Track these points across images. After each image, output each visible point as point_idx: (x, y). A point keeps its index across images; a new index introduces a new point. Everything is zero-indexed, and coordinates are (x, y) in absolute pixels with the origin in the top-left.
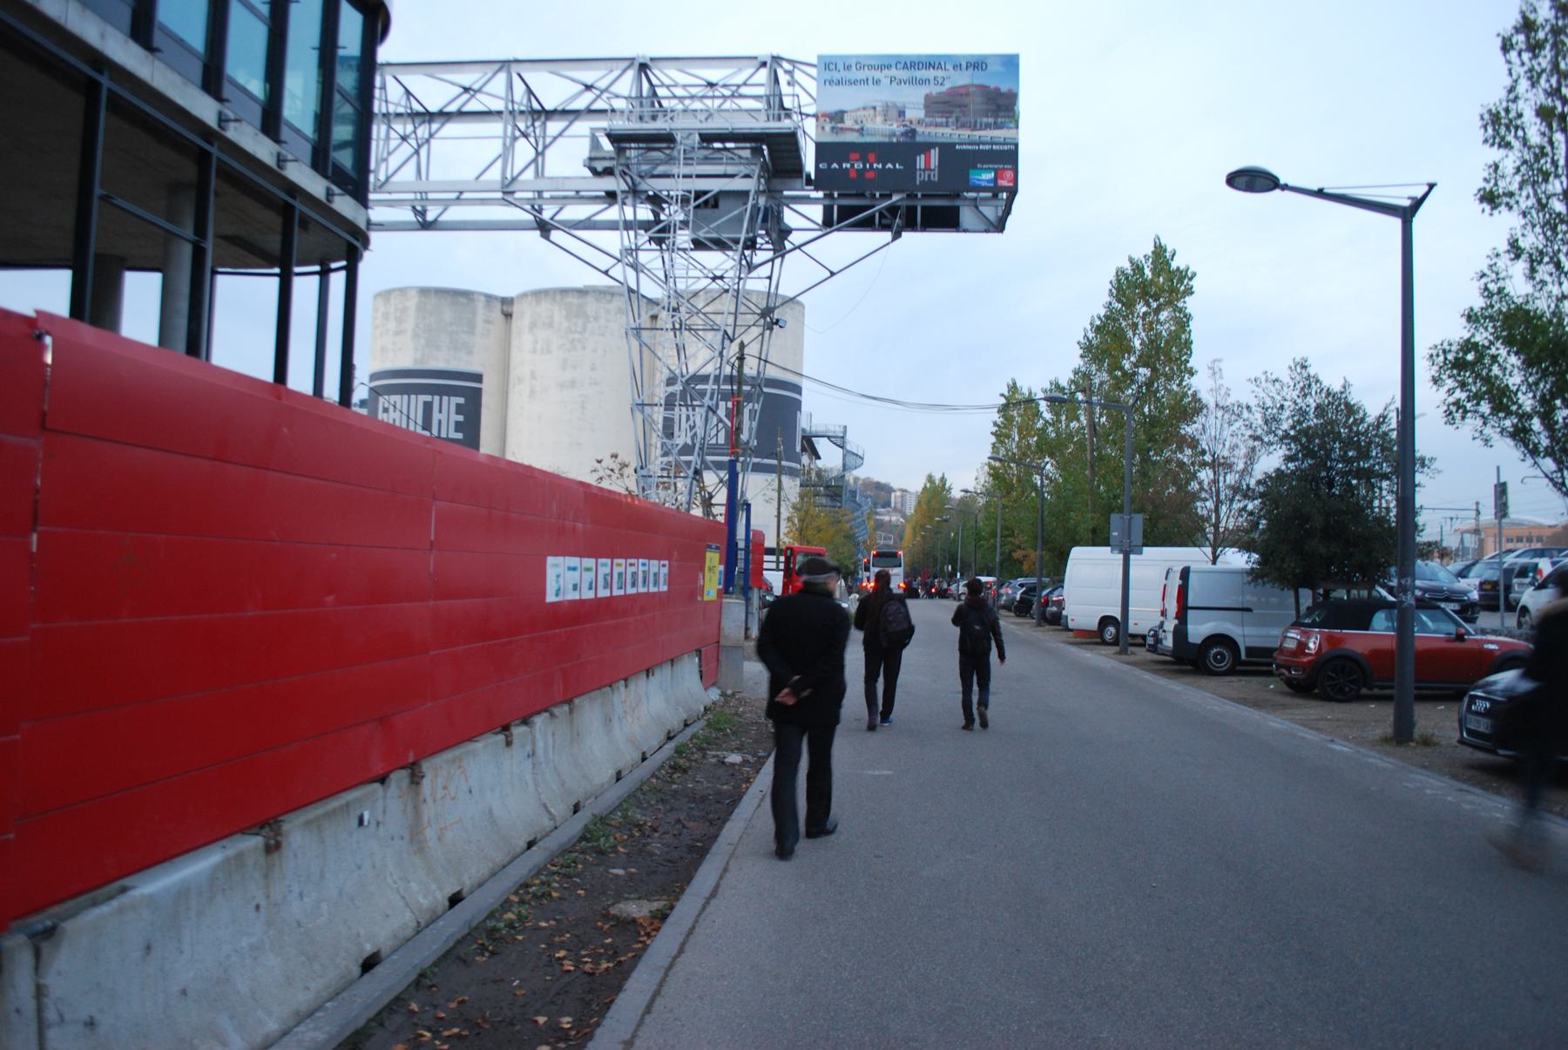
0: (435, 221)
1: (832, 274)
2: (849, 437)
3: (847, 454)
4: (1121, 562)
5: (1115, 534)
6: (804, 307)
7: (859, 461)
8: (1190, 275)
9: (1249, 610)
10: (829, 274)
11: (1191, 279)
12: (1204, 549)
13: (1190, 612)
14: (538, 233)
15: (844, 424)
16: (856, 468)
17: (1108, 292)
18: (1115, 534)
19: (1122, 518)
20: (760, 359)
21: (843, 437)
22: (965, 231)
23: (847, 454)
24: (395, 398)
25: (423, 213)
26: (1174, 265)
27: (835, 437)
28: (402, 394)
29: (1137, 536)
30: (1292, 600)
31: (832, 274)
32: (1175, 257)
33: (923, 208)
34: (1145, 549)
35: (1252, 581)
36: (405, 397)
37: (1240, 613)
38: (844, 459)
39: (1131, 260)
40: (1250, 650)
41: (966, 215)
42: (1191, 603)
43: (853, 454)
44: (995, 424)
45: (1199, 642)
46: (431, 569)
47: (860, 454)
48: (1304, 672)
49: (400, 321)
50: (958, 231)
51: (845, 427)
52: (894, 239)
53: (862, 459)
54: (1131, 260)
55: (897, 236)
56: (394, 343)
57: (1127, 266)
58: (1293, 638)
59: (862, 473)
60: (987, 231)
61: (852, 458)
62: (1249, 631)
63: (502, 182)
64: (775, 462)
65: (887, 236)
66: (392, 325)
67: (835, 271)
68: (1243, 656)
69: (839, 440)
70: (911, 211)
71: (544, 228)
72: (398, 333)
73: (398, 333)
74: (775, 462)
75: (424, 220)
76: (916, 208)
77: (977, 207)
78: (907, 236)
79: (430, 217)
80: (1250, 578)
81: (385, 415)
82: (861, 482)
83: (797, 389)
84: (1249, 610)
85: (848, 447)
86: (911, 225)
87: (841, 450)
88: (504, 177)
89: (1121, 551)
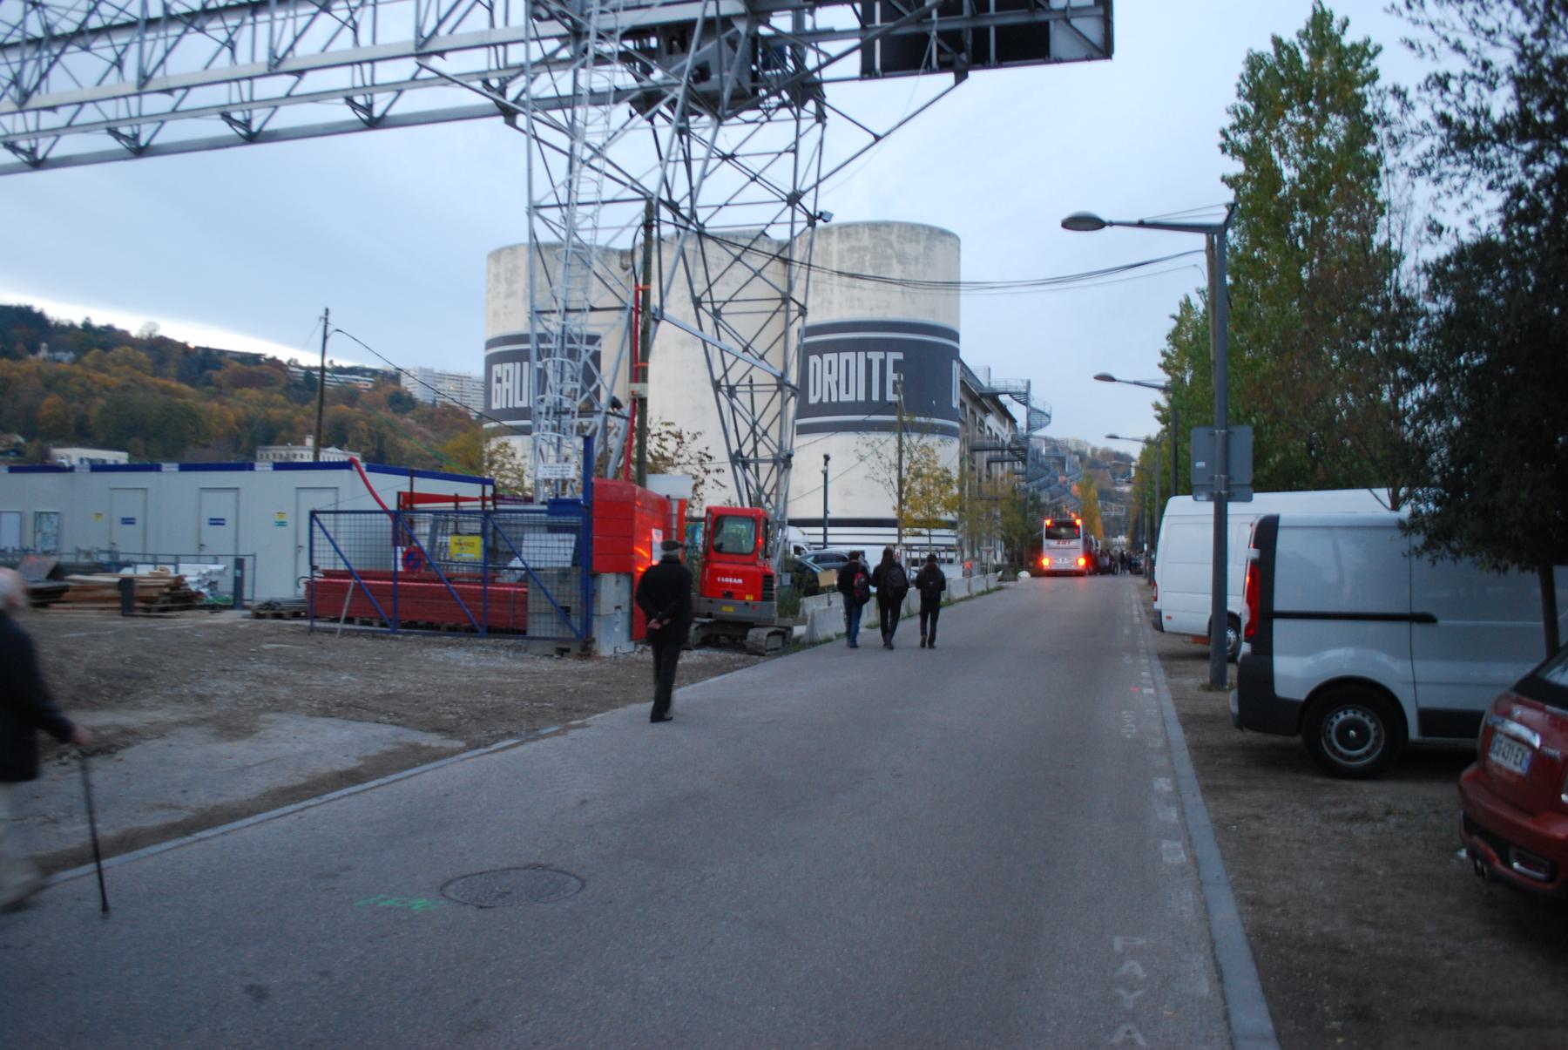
0: (383, 116)
1: (877, 138)
2: (1033, 393)
3: (1032, 412)
4: (1211, 520)
5: (1200, 464)
6: (959, 240)
7: (1045, 419)
8: (1371, 50)
9: (1426, 619)
10: (872, 139)
11: (1372, 57)
12: (1377, 491)
13: (1278, 625)
14: (501, 119)
15: (1027, 378)
16: (1041, 427)
17: (1235, 90)
18: (1200, 464)
19: (1213, 434)
20: (810, 265)
21: (1026, 394)
22: (1059, 61)
23: (1032, 412)
24: (509, 366)
25: (368, 108)
26: (1346, 41)
27: (1016, 393)
28: (514, 361)
29: (1243, 470)
30: (1537, 592)
31: (877, 138)
32: (1348, 30)
33: (999, 29)
34: (1256, 496)
35: (1428, 546)
36: (518, 364)
37: (1403, 627)
38: (1028, 418)
39: (1277, 42)
40: (1426, 716)
41: (1059, 39)
42: (1279, 605)
43: (1040, 412)
44: (1164, 354)
45: (1301, 695)
46: (641, 551)
47: (1047, 411)
48: (1550, 879)
49: (510, 282)
50: (1049, 62)
51: (1029, 383)
52: (958, 81)
53: (1049, 416)
54: (1277, 42)
55: (961, 77)
56: (505, 307)
57: (1268, 49)
58: (1518, 739)
59: (1052, 431)
60: (1089, 58)
61: (1039, 417)
62: (1429, 669)
63: (417, 41)
64: (893, 418)
65: (949, 78)
66: (503, 287)
67: (880, 133)
68: (1414, 733)
69: (1023, 398)
70: (981, 35)
71: (509, 114)
72: (509, 295)
73: (509, 295)
74: (893, 418)
75: (371, 117)
76: (987, 30)
77: (1068, 21)
78: (975, 76)
79: (377, 112)
80: (1419, 540)
81: (499, 385)
82: (1098, 452)
83: (955, 336)
84: (1426, 619)
85: (1033, 404)
86: (981, 60)
87: (1024, 407)
88: (419, 31)
89: (1211, 497)
